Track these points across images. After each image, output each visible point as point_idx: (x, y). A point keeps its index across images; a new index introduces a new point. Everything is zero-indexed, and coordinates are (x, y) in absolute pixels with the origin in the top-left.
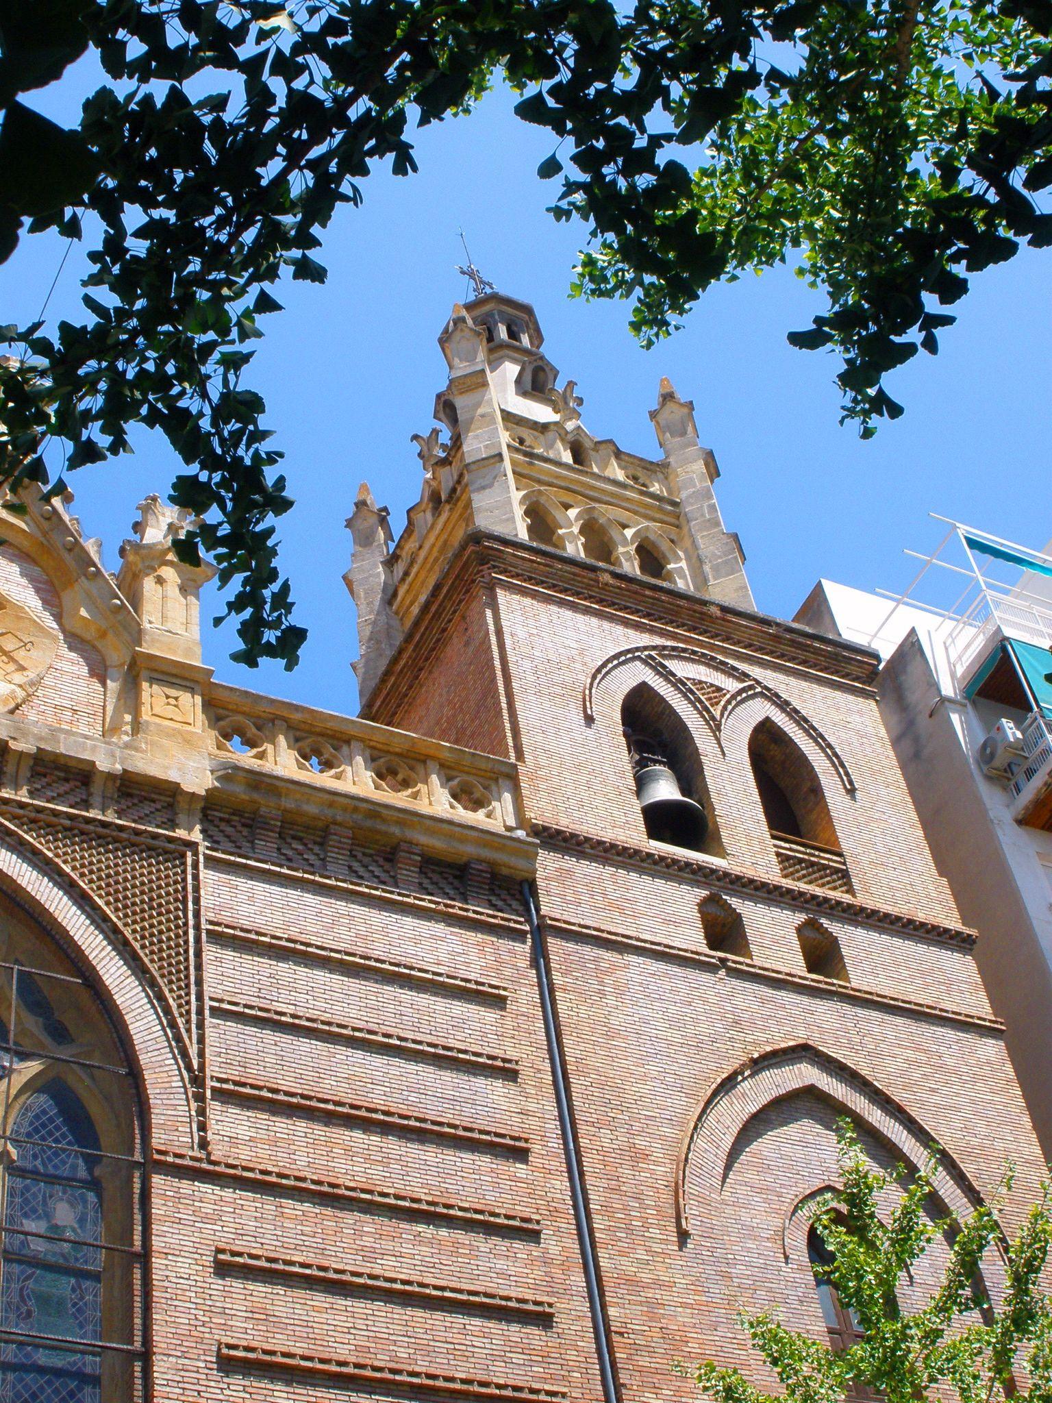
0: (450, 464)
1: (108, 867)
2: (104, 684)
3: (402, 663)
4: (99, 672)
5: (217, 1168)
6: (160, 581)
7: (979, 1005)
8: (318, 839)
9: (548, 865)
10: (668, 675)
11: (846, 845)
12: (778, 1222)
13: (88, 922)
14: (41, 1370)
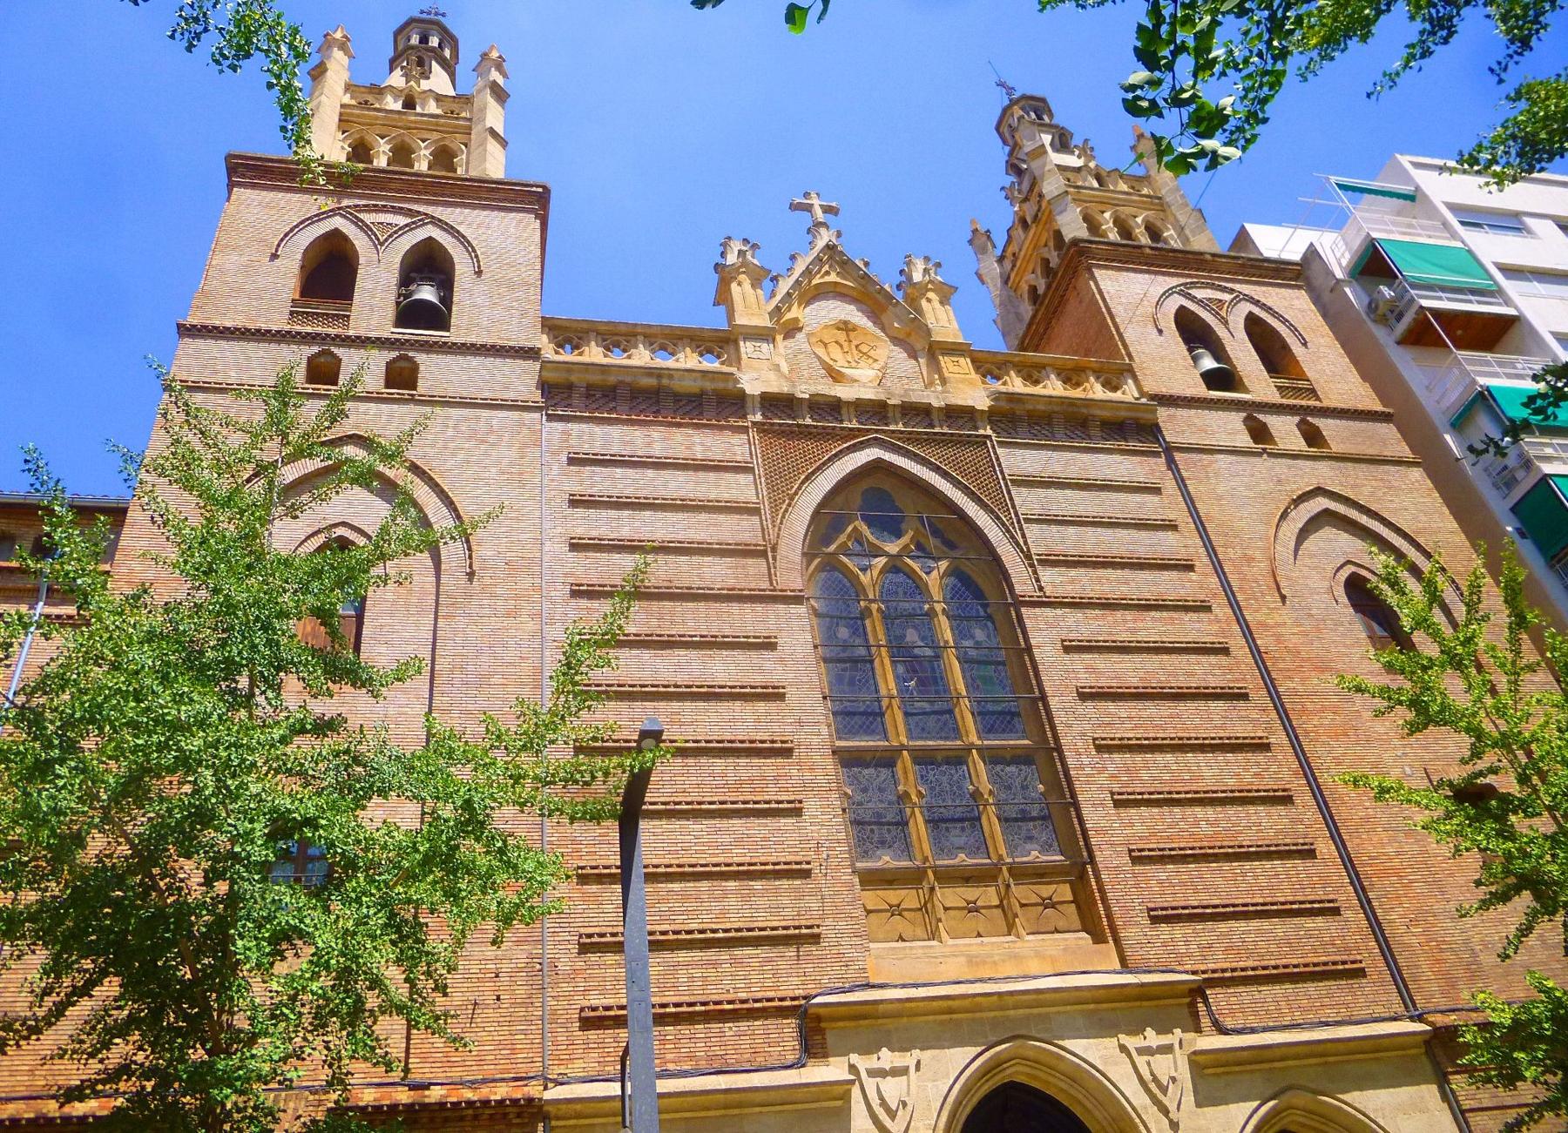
4: (913, 355)
6: (929, 300)
7: (1404, 451)
9: (1163, 414)
10: (1192, 298)
11: (1309, 374)
12: (1326, 584)
14: (993, 713)
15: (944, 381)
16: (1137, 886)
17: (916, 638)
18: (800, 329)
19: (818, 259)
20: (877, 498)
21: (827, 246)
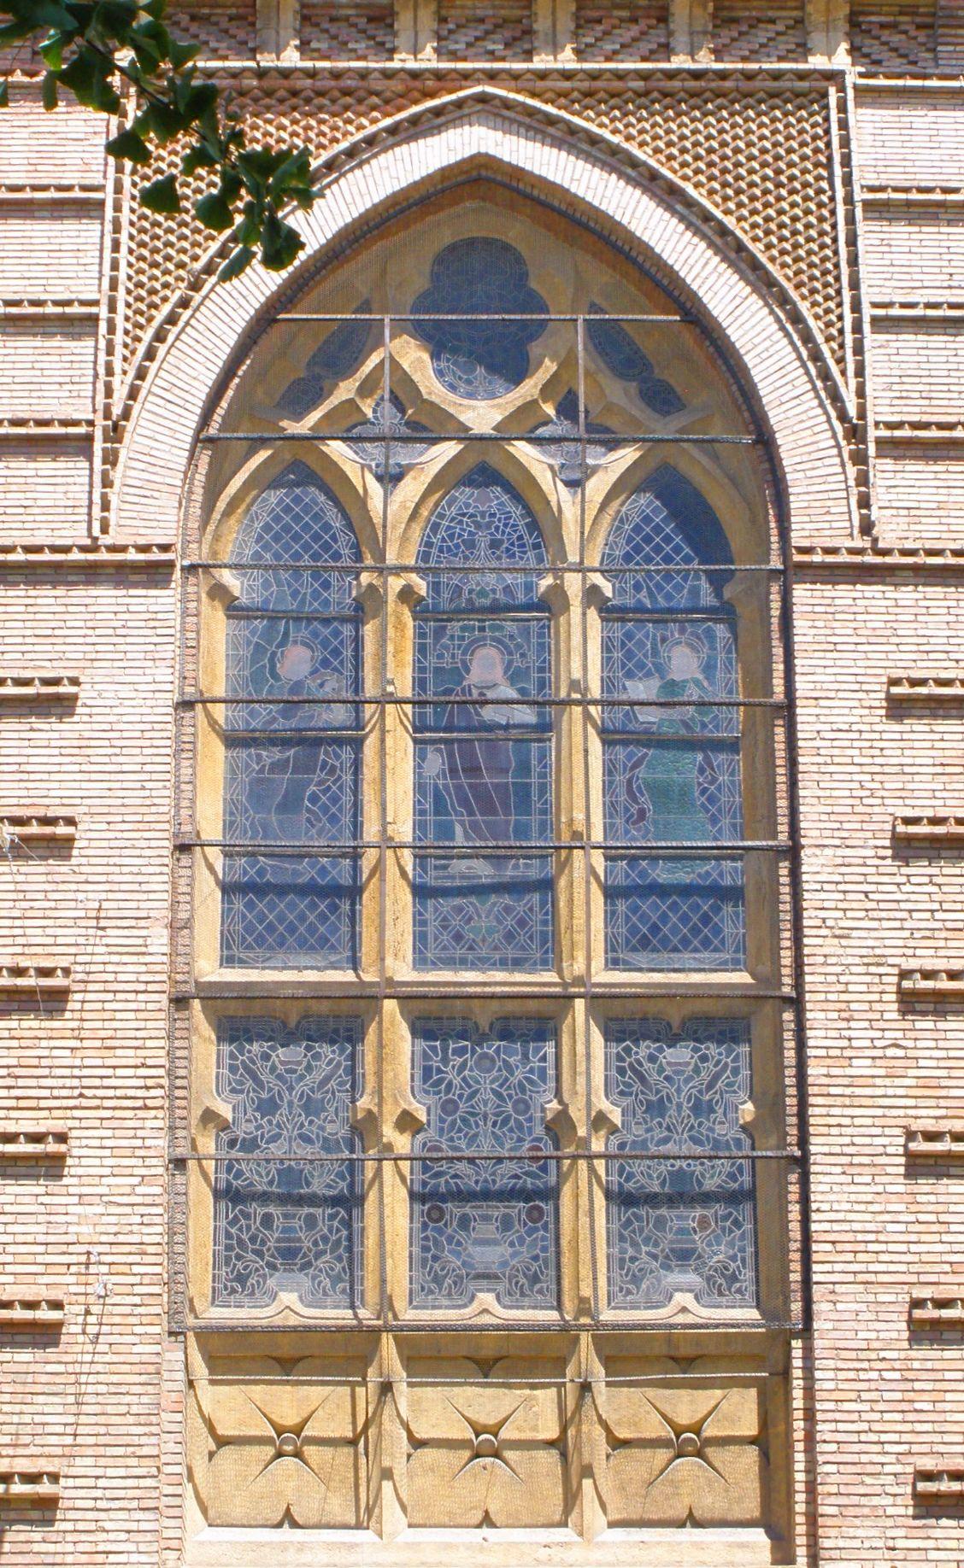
1: (709, 137)
5: (888, 560)
13: (682, 227)
14: (662, 891)
16: (907, 1407)
17: (498, 674)
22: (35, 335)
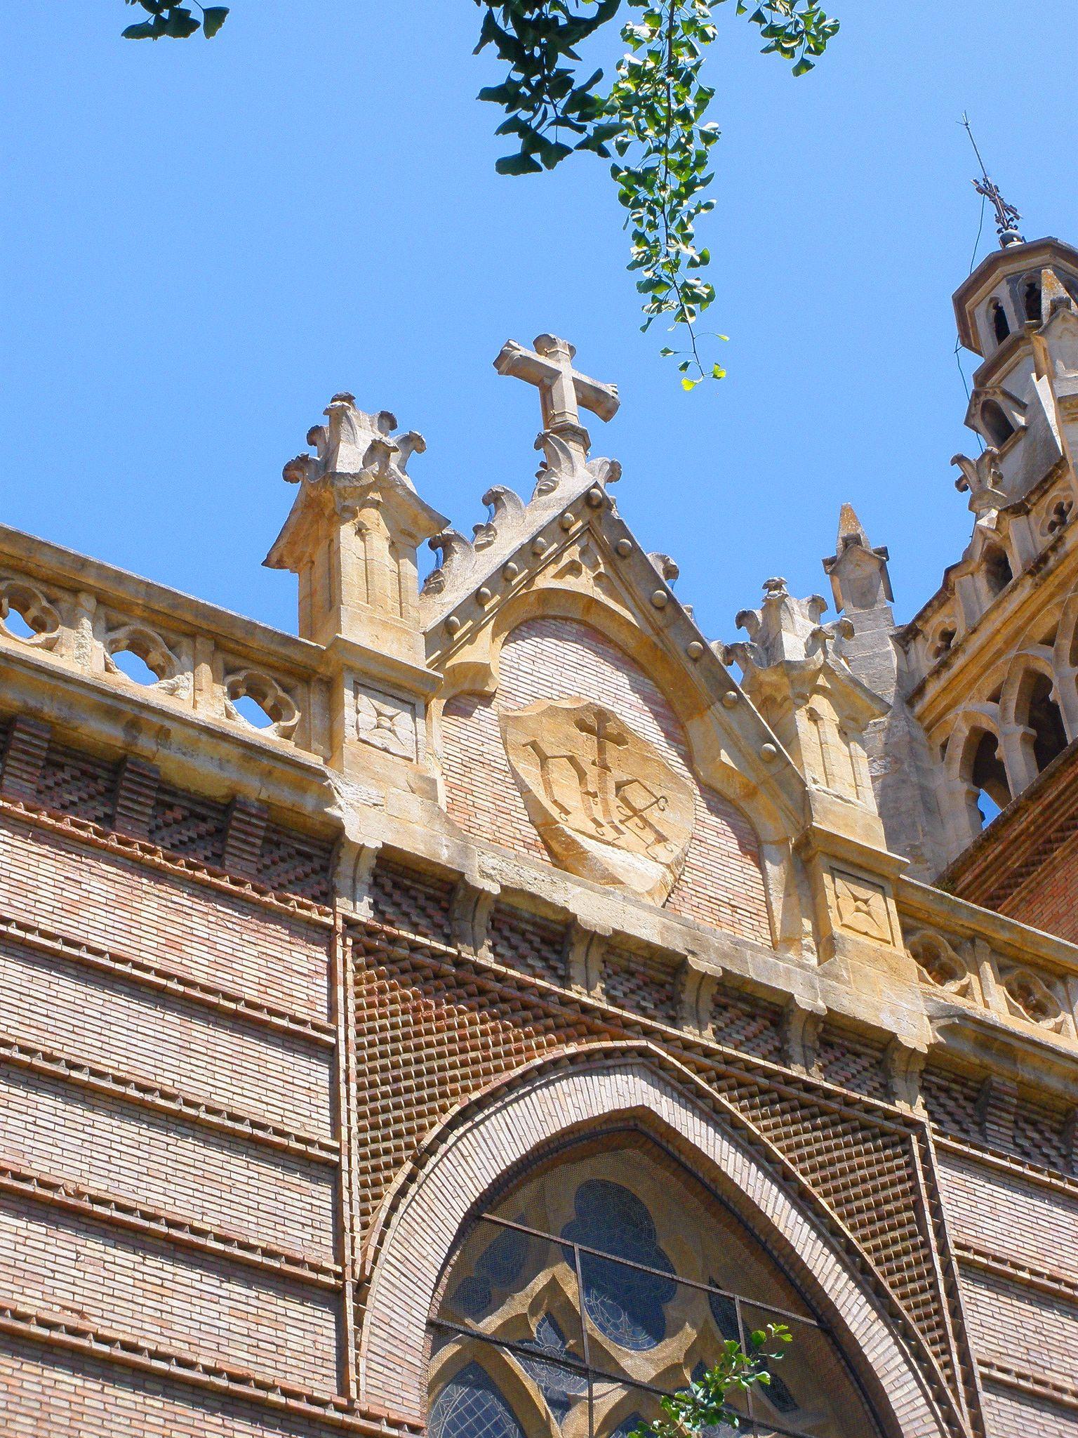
0: (1028, 513)
2: (763, 870)
3: (1018, 828)
4: (754, 848)
6: (814, 717)
8: (1055, 1125)
15: (827, 946)
18: (487, 699)
19: (560, 526)
20: (610, 1216)
21: (587, 498)
22: (277, 1165)
